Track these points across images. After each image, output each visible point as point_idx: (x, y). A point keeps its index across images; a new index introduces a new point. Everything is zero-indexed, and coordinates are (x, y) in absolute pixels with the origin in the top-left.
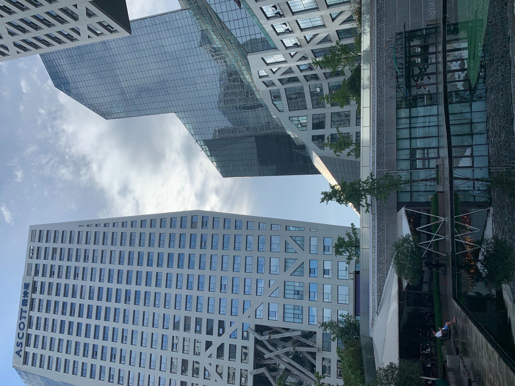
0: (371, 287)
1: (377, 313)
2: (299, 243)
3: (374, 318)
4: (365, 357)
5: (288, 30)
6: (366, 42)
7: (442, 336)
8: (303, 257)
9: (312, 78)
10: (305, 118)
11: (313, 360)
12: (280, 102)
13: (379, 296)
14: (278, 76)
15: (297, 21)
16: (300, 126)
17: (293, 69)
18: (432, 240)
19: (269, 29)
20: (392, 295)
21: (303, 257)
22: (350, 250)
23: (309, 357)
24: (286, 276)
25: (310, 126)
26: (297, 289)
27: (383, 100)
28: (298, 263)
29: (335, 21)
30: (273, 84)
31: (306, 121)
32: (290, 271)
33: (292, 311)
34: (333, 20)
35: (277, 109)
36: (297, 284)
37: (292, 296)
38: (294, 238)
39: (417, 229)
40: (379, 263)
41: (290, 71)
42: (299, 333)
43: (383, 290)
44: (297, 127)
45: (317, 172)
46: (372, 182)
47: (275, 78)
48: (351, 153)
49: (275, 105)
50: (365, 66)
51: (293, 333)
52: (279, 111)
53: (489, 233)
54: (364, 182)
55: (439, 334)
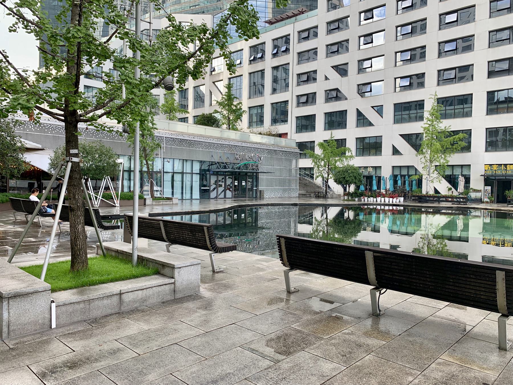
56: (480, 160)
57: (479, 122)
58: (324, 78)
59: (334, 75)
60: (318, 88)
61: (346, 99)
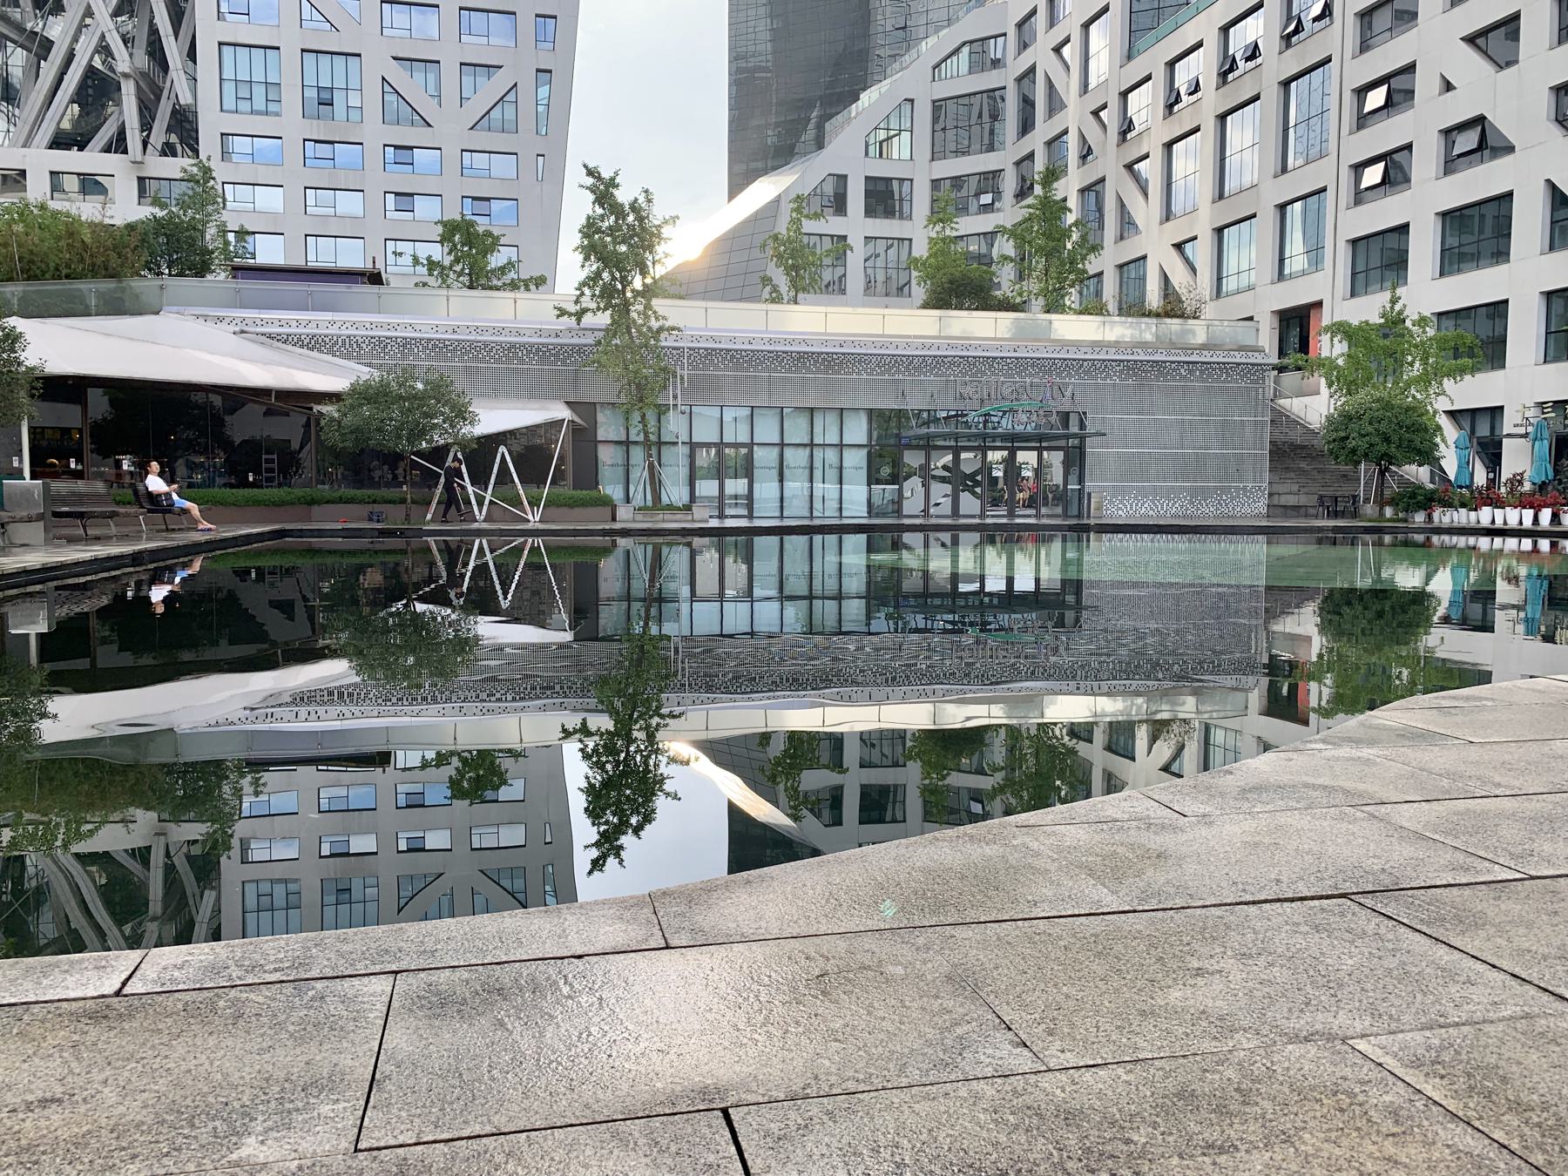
0: (328, 316)
1: (243, 332)
2: (496, 114)
3: (224, 325)
4: (90, 288)
5: (1178, 100)
6: (1074, 329)
7: (150, 494)
8: (451, 126)
9: (1023, 179)
10: (906, 155)
11: (102, 143)
12: (964, 68)
13: (299, 339)
14: (1046, 63)
15: (1197, 129)
16: (882, 135)
17: (1057, 117)
18: (470, 489)
19: (1187, 36)
20: (293, 372)
21: (451, 126)
22: (458, 268)
23: (106, 133)
24: (377, 64)
25: (880, 169)
26: (338, 98)
27: (899, 371)
28: (427, 108)
29: (1173, 253)
30: (1024, 46)
31: (895, 156)
32: (397, 75)
33: (258, 76)
34: (1179, 247)
35: (945, 60)
36: (354, 101)
37: (310, 80)
38: (511, 97)
39: (502, 449)
40: (406, 343)
41: (1055, 104)
42: (185, 99)
43: (321, 351)
44: (881, 129)
45: (735, 189)
46: (650, 329)
47: (1040, 54)
48: (768, 289)
49: (956, 51)
50: (1008, 323)
51: (183, 77)
52: (938, 65)
53: (488, 629)
54: (648, 307)
55: (155, 483)
56: (1526, 383)
57: (1528, 274)
58: (1437, 84)
59: (1469, 67)
60: (1419, 126)
61: (1510, 149)
